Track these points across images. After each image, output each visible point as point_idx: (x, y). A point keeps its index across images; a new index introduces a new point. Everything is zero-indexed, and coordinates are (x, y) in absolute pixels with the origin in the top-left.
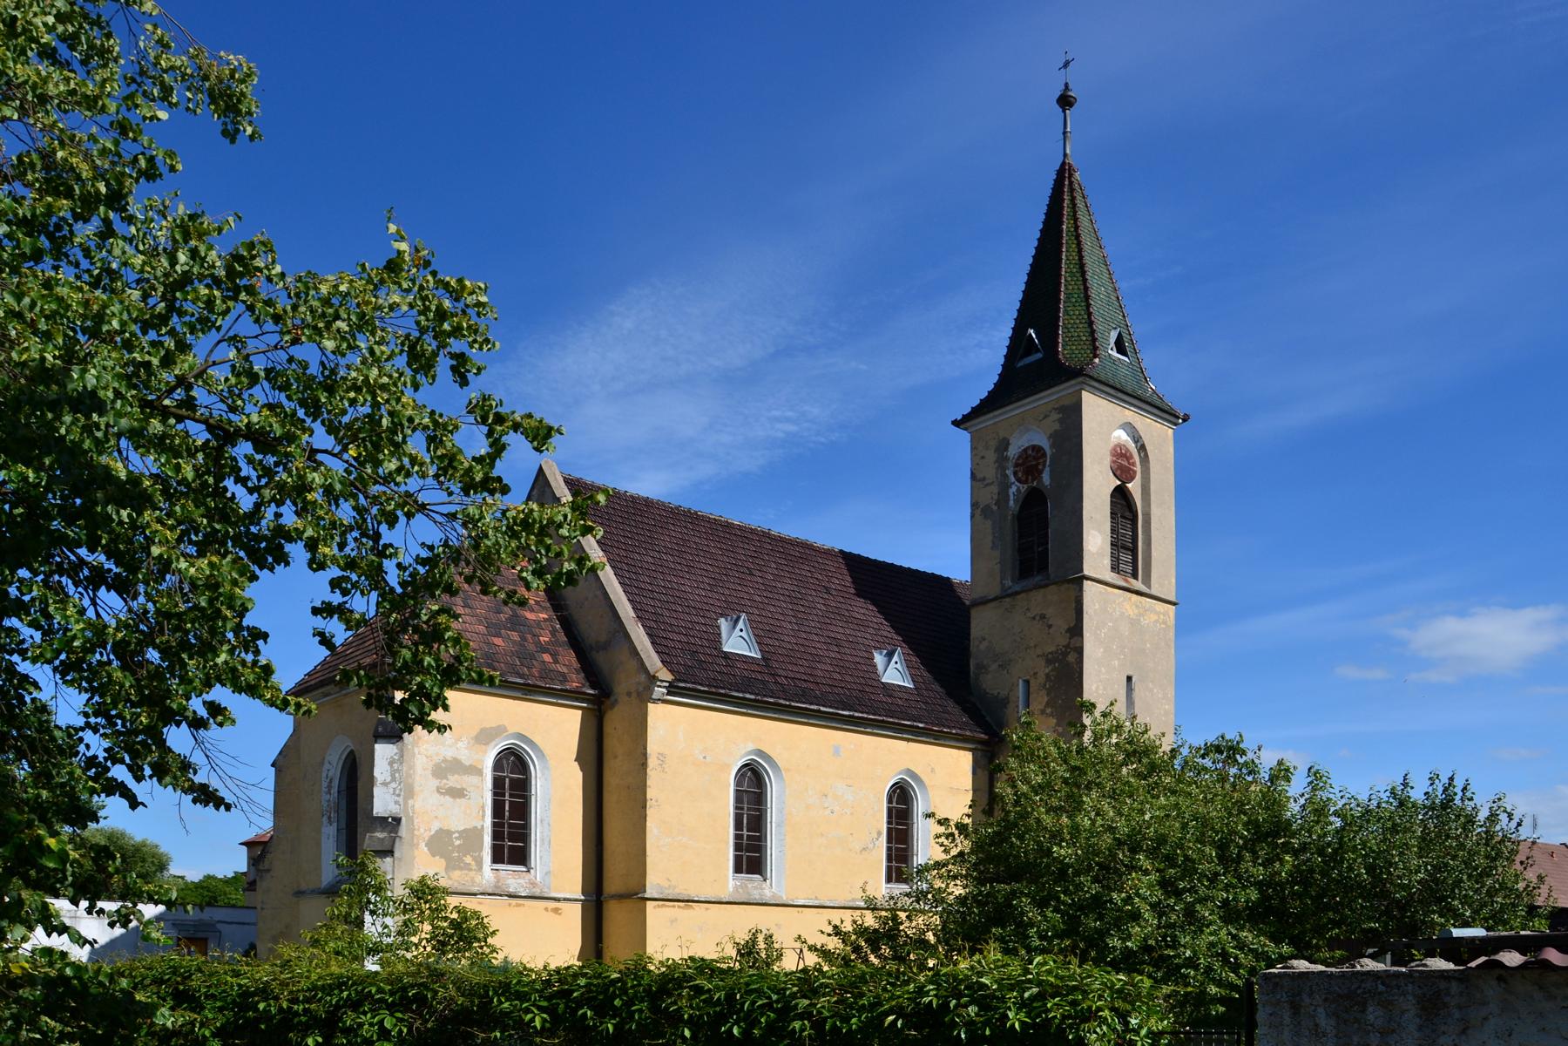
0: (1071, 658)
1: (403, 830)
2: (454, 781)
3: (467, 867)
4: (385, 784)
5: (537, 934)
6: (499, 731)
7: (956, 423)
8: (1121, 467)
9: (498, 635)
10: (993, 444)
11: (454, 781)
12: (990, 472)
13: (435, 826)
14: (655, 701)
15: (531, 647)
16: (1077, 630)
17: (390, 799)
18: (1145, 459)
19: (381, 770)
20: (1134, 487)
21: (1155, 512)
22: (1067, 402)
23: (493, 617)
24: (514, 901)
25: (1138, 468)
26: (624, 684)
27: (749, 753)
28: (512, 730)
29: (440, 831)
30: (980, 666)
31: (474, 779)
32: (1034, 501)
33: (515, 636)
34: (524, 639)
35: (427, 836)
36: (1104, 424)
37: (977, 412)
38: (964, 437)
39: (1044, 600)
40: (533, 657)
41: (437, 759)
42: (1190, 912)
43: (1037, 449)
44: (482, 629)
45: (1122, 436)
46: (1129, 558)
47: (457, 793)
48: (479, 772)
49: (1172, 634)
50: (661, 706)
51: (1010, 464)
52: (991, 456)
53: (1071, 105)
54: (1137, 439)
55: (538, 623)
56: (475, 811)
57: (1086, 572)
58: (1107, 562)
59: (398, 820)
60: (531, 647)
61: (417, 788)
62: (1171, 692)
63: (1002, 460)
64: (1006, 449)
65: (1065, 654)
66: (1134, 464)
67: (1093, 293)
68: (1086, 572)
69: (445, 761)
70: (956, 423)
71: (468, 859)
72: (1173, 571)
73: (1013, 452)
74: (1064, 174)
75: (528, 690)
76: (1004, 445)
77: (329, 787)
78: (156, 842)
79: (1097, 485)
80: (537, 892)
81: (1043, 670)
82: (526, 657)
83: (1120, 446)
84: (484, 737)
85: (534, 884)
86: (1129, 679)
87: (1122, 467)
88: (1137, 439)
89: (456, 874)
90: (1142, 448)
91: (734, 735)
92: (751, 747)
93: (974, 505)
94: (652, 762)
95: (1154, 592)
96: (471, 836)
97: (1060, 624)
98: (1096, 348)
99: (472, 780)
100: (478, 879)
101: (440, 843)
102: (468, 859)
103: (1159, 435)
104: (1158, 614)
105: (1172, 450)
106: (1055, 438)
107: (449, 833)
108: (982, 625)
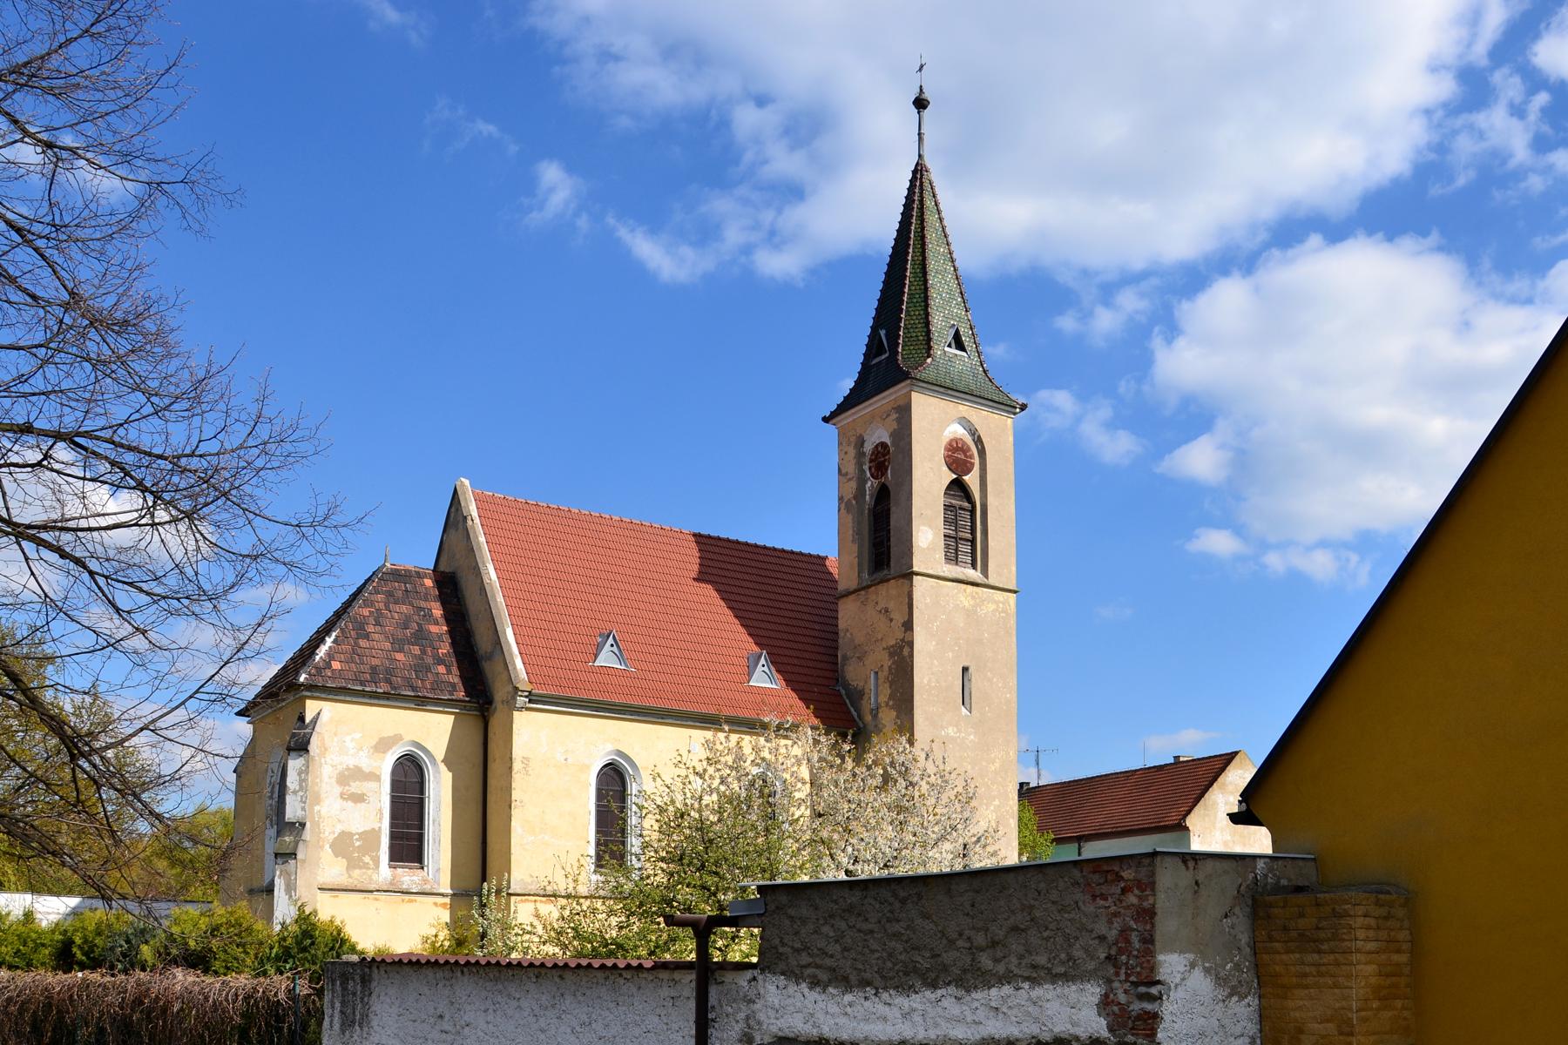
0: (906, 652)
1: (307, 834)
2: (356, 787)
3: (366, 866)
4: (295, 792)
5: (396, 919)
6: (397, 739)
7: (826, 420)
8: (956, 461)
9: (400, 651)
10: (853, 439)
11: (356, 787)
12: (851, 468)
13: (339, 829)
14: (520, 709)
15: (429, 660)
16: (908, 625)
17: (299, 806)
18: (982, 453)
19: (292, 781)
20: (972, 480)
21: (992, 501)
22: (901, 403)
23: (399, 633)
24: (407, 897)
25: (976, 461)
26: (500, 694)
27: (610, 753)
28: (408, 738)
29: (343, 833)
30: (845, 658)
31: (373, 785)
32: (883, 494)
33: (416, 650)
34: (424, 652)
35: (332, 837)
36: (935, 423)
37: (843, 408)
38: (831, 430)
39: (886, 594)
40: (428, 669)
41: (340, 768)
42: (1116, 915)
43: (883, 445)
44: (388, 646)
45: (957, 431)
46: (968, 549)
47: (359, 798)
48: (377, 778)
49: (1013, 622)
50: (525, 714)
51: (867, 459)
52: (852, 452)
53: (925, 107)
54: (973, 432)
55: (440, 636)
56: (376, 814)
57: (915, 569)
58: (940, 554)
59: (303, 825)
60: (429, 660)
61: (323, 796)
62: (1013, 682)
63: (860, 454)
64: (862, 445)
65: (901, 648)
66: (971, 457)
67: (933, 293)
68: (915, 569)
69: (348, 769)
70: (826, 420)
71: (367, 859)
72: (1014, 560)
73: (868, 447)
74: (919, 172)
75: (420, 702)
76: (861, 442)
77: (272, 792)
78: (380, 944)
79: (928, 481)
80: (427, 888)
81: (887, 663)
82: (421, 668)
83: (956, 440)
84: (383, 745)
85: (425, 881)
86: (965, 670)
87: (957, 458)
88: (973, 432)
89: (356, 873)
90: (979, 441)
91: (593, 740)
92: (610, 747)
93: (841, 499)
94: (517, 766)
95: (991, 581)
96: (370, 837)
97: (899, 618)
98: (930, 348)
99: (370, 786)
100: (375, 877)
101: (342, 845)
102: (367, 859)
103: (998, 429)
104: (997, 602)
105: (1011, 439)
106: (893, 435)
107: (351, 835)
108: (848, 613)
